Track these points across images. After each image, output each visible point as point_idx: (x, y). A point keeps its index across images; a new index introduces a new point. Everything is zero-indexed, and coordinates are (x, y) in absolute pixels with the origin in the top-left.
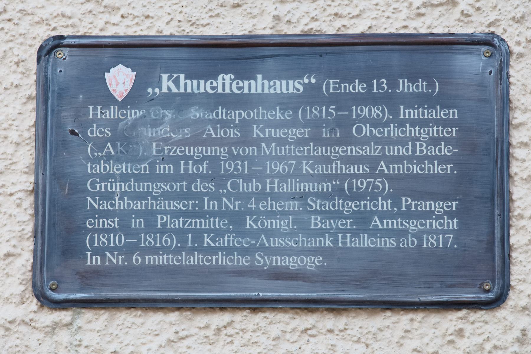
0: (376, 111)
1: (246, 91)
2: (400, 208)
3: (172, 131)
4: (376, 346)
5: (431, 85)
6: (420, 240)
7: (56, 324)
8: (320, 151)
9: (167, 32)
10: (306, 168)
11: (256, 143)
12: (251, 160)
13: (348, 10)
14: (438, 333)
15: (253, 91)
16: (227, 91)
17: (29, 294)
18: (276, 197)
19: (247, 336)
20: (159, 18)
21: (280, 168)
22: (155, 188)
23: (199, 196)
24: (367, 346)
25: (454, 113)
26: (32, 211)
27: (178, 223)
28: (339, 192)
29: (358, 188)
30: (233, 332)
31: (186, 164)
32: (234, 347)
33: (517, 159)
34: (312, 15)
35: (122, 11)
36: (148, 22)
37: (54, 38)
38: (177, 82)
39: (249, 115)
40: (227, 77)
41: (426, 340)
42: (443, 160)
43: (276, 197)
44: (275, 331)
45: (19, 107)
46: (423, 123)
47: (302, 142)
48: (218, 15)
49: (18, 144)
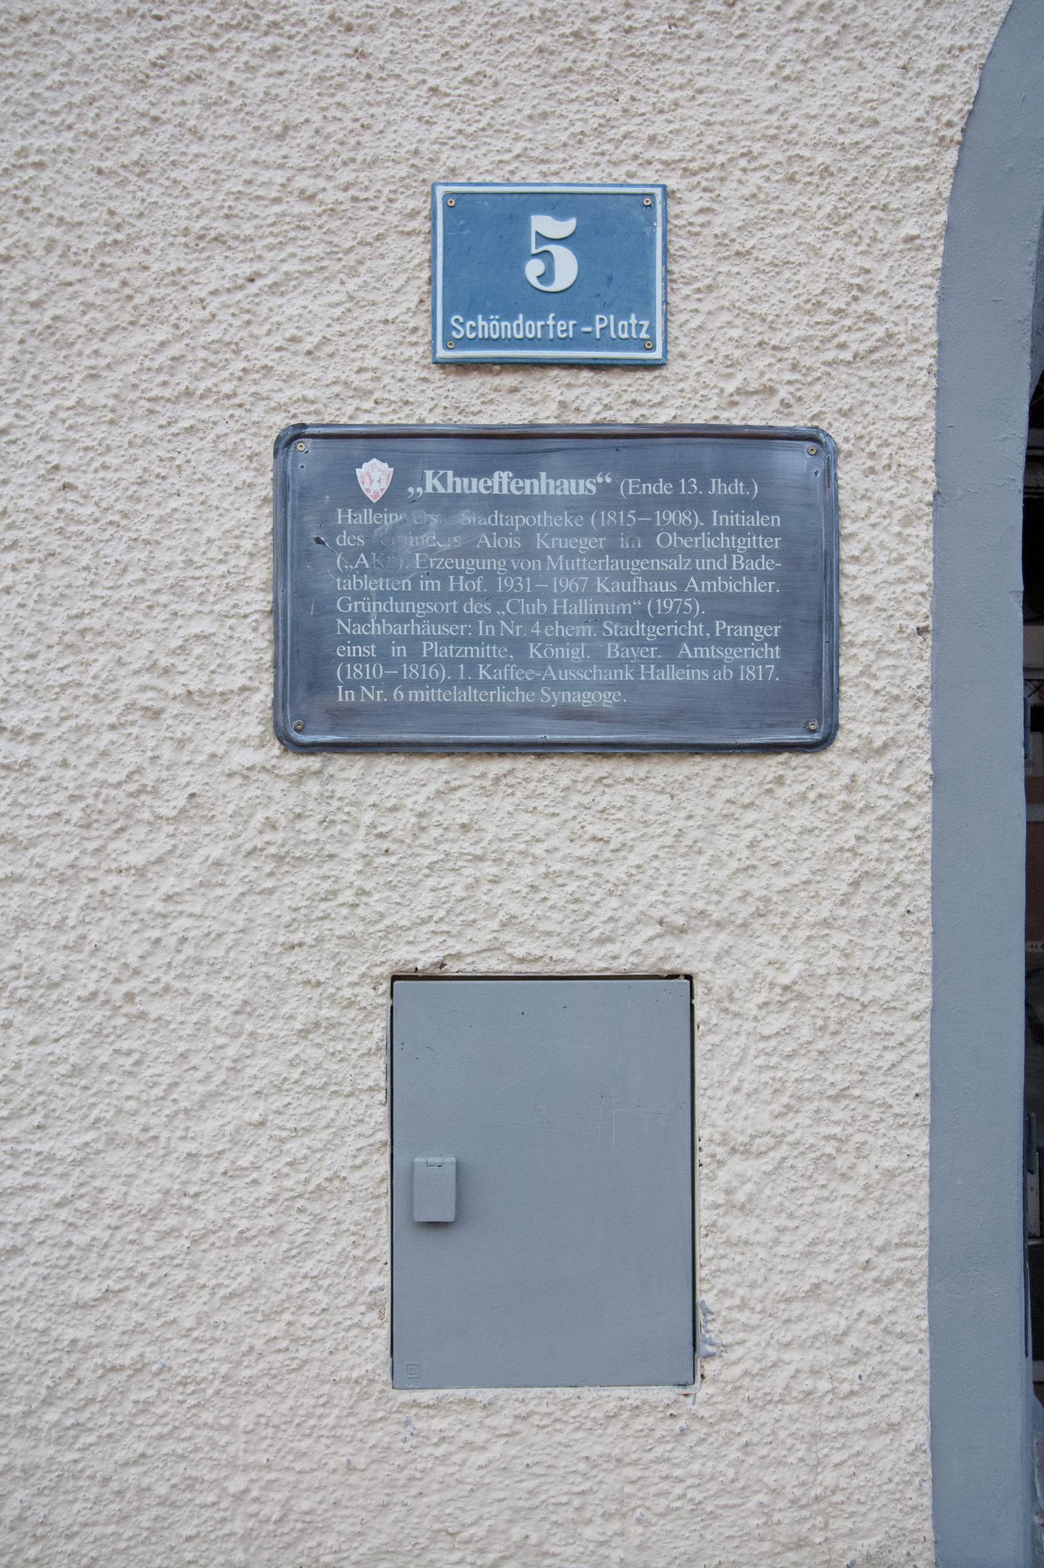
0: (684, 517)
1: (528, 492)
2: (713, 633)
3: (438, 539)
4: (683, 796)
5: (748, 486)
6: (737, 672)
7: (303, 771)
8: (618, 564)
9: (430, 420)
10: (600, 585)
11: (541, 554)
12: (535, 576)
13: (648, 396)
14: (755, 781)
15: (536, 492)
16: (505, 491)
17: (270, 736)
18: (564, 620)
19: (531, 786)
20: (421, 404)
21: (569, 585)
22: (418, 608)
23: (473, 619)
24: (672, 797)
25: (776, 521)
26: (270, 636)
27: (448, 651)
28: (641, 614)
29: (664, 610)
30: (513, 781)
31: (456, 580)
32: (515, 799)
33: (847, 576)
34: (606, 401)
35: (376, 396)
36: (407, 410)
37: (294, 426)
38: (443, 480)
39: (531, 521)
40: (505, 475)
41: (741, 789)
42: (763, 576)
43: (564, 620)
44: (564, 780)
45: (252, 510)
46: (740, 532)
47: (595, 554)
48: (491, 401)
49: (252, 555)
